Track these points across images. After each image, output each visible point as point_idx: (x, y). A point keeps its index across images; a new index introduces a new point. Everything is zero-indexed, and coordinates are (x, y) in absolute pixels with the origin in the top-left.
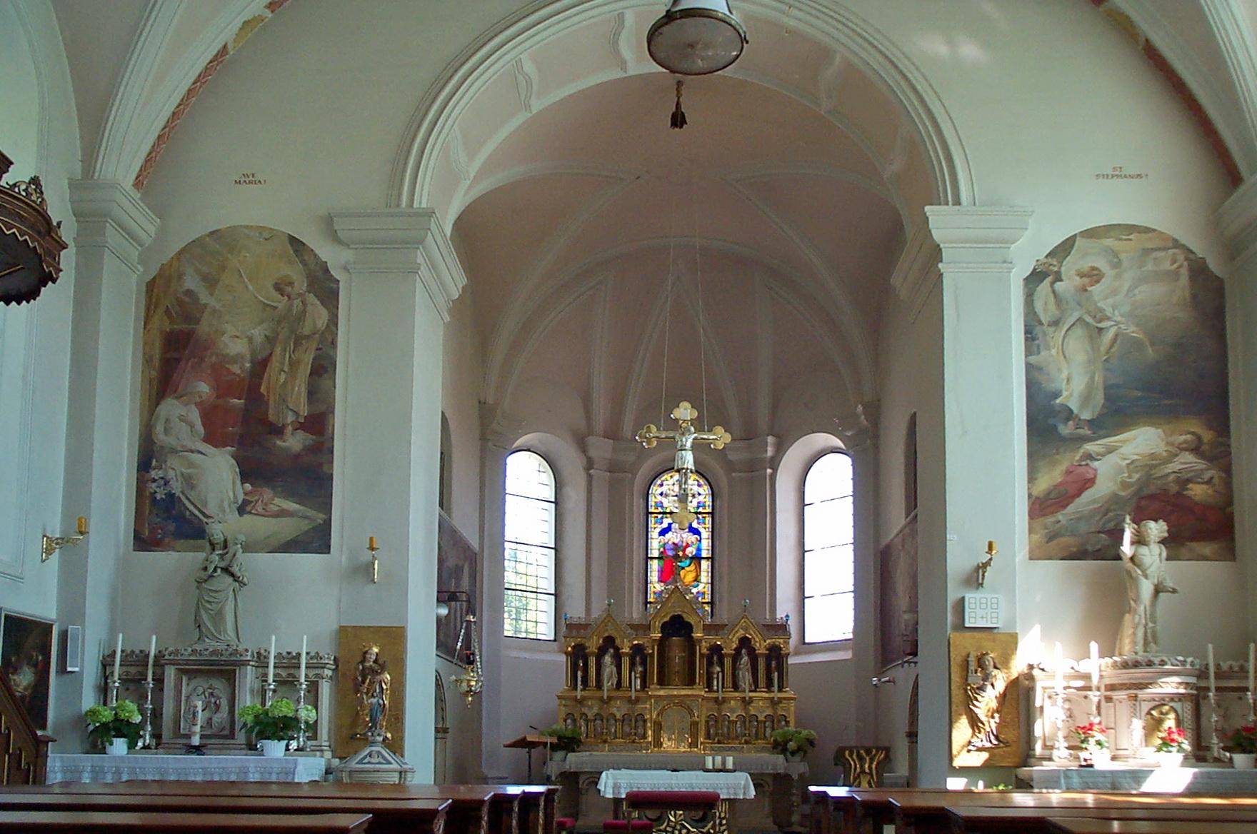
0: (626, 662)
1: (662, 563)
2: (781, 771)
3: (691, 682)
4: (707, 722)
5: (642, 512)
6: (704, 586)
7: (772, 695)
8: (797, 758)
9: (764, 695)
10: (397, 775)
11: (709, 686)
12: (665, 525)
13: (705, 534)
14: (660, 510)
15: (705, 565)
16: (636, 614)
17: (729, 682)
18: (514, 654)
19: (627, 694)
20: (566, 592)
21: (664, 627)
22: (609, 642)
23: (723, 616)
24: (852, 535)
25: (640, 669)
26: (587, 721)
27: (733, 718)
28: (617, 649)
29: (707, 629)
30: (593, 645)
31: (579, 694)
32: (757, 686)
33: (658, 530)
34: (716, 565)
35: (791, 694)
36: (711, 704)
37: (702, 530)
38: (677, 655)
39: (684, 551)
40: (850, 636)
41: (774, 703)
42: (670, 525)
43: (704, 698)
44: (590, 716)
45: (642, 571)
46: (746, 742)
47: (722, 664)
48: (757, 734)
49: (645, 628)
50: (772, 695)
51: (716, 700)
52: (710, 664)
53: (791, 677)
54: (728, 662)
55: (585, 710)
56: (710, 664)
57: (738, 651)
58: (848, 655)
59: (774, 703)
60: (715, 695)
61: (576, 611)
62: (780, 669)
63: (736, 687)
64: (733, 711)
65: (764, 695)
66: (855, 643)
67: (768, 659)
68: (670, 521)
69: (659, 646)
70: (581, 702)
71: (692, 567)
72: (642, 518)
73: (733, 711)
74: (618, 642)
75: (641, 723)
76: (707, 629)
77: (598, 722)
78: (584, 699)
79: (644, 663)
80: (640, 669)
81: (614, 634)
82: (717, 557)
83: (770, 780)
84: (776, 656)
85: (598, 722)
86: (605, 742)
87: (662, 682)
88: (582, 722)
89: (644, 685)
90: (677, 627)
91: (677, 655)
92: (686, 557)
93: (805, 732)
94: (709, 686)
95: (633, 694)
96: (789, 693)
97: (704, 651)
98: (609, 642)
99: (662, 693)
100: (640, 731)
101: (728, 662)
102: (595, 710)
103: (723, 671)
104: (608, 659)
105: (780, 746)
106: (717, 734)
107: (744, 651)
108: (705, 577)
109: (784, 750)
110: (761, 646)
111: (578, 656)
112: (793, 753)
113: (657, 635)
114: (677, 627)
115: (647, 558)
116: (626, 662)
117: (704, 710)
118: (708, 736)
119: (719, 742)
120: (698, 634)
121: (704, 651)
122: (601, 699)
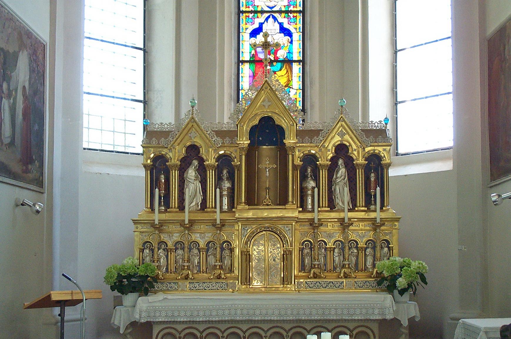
0: (211, 176)
1: (253, 66)
2: (389, 317)
3: (282, 201)
4: (301, 250)
5: (234, 10)
6: (295, 94)
7: (373, 215)
8: (406, 296)
9: (362, 215)
10: (237, 229)
11: (303, 204)
12: (256, 26)
13: (297, 36)
14: (251, 9)
15: (296, 68)
16: (224, 115)
17: (325, 201)
18: (96, 169)
19: (178, 216)
20: (155, 98)
21: (253, 132)
22: (193, 151)
23: (315, 120)
24: (450, 29)
25: (227, 185)
26: (166, 250)
27: (330, 245)
28: (201, 161)
29: (301, 134)
30: (175, 156)
31: (157, 217)
32: (355, 205)
33: (249, 31)
34: (307, 68)
35: (391, 212)
36: (306, 228)
37: (293, 30)
38: (267, 165)
39: (275, 53)
40: (451, 144)
41: (376, 225)
42: (261, 24)
43: (298, 221)
44: (170, 245)
45: (234, 77)
46: (346, 276)
47: (316, 179)
48: (357, 264)
49: (232, 134)
50: (373, 215)
51: (311, 222)
52: (304, 178)
53: (392, 189)
54: (323, 174)
55: (164, 237)
56: (304, 178)
57: (334, 160)
58: (447, 166)
59: (376, 225)
60: (309, 216)
61: (165, 116)
62: (381, 181)
63: (332, 206)
64: (330, 236)
65: (362, 215)
66: (459, 152)
67: (367, 169)
68: (262, 20)
69: (247, 156)
70: (159, 227)
71: (284, 71)
72: (234, 17)
73: (330, 234)
74: (203, 151)
75: (227, 252)
76: (301, 134)
77: (180, 252)
78: (162, 223)
79: (231, 178)
80: (227, 185)
81: (198, 142)
82: (308, 61)
83: (375, 327)
84: (376, 166)
85: (180, 252)
86: (187, 278)
87: (252, 201)
88: (161, 252)
89: (232, 205)
90: (267, 131)
91: (267, 165)
92: (277, 60)
93: (415, 264)
94: (303, 204)
95: (218, 216)
96: (391, 212)
97: (298, 162)
98: (193, 151)
99: (250, 214)
100: (227, 262)
101: (323, 174)
102: (176, 237)
103: (318, 186)
104: (191, 173)
105: (387, 283)
106: (312, 267)
107: (340, 162)
108: (296, 83)
109: (391, 288)
110: (359, 157)
111: (157, 168)
112: (402, 292)
113: (245, 142)
114: (267, 131)
115: (240, 62)
116: (211, 176)
117: (298, 234)
118: (302, 268)
119: (315, 276)
120: (290, 140)
121: (298, 162)
122: (182, 223)
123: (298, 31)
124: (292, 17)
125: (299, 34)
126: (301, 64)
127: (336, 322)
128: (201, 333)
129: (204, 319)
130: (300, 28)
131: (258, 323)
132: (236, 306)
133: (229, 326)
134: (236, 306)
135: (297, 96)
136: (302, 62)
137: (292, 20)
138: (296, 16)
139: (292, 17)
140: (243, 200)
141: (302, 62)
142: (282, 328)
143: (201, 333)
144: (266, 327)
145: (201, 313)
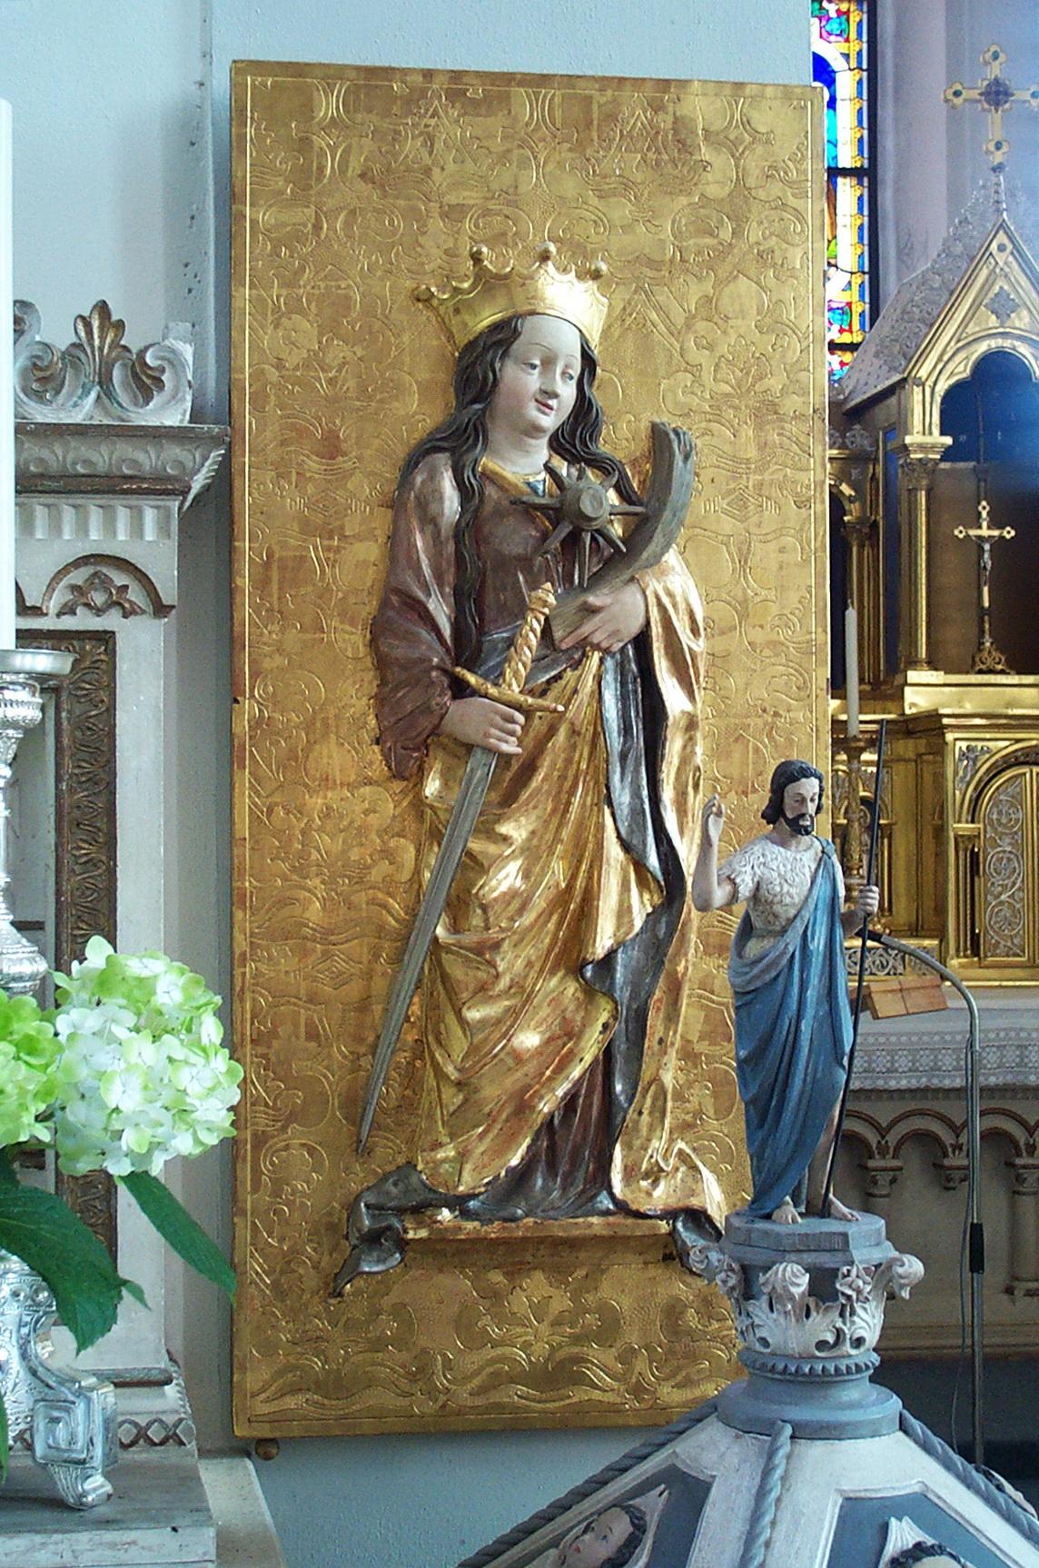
13: (847, 83)
82: (888, 173)
123: (853, 64)
124: (833, 14)
125: (856, 75)
126: (866, 180)
127: (914, 1098)
128: (883, 1132)
129: (914, 1084)
130: (859, 53)
131: (1004, 1097)
132: (1023, 1035)
133: (913, 1106)
134: (1023, 1035)
135: (854, 296)
136: (868, 174)
137: (834, 26)
138: (847, 13)
139: (833, 14)
140: (923, 653)
141: (868, 174)
142: (942, 1118)
143: (883, 1132)
144: (884, 1113)
145: (903, 1063)
